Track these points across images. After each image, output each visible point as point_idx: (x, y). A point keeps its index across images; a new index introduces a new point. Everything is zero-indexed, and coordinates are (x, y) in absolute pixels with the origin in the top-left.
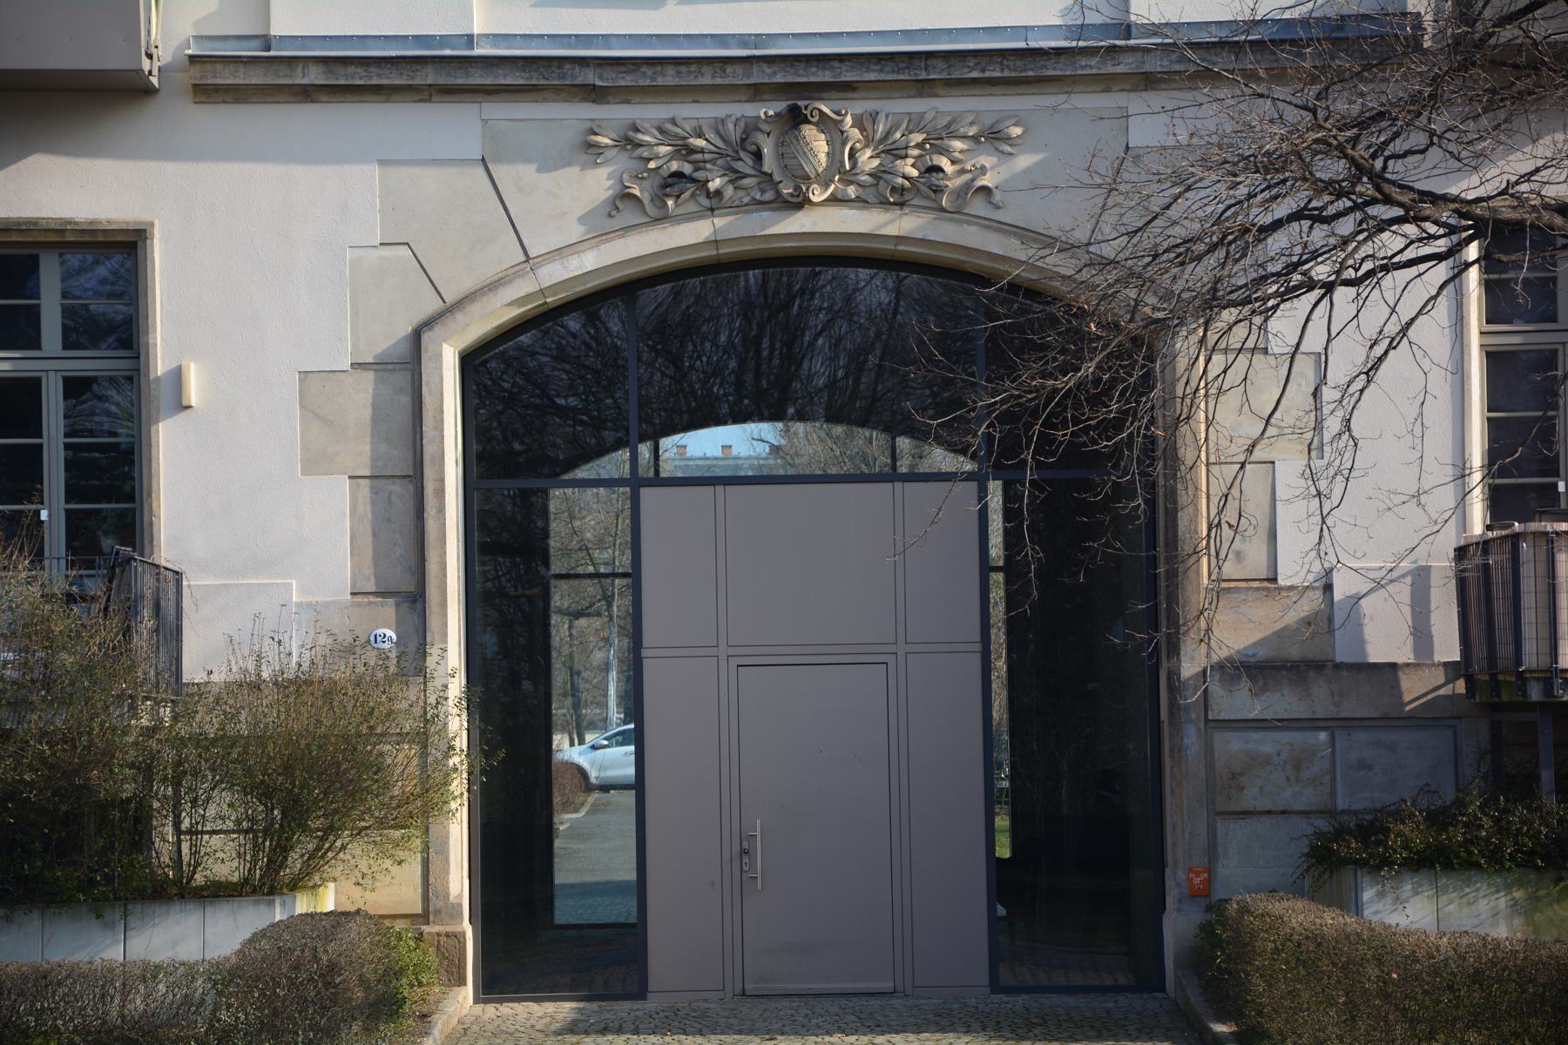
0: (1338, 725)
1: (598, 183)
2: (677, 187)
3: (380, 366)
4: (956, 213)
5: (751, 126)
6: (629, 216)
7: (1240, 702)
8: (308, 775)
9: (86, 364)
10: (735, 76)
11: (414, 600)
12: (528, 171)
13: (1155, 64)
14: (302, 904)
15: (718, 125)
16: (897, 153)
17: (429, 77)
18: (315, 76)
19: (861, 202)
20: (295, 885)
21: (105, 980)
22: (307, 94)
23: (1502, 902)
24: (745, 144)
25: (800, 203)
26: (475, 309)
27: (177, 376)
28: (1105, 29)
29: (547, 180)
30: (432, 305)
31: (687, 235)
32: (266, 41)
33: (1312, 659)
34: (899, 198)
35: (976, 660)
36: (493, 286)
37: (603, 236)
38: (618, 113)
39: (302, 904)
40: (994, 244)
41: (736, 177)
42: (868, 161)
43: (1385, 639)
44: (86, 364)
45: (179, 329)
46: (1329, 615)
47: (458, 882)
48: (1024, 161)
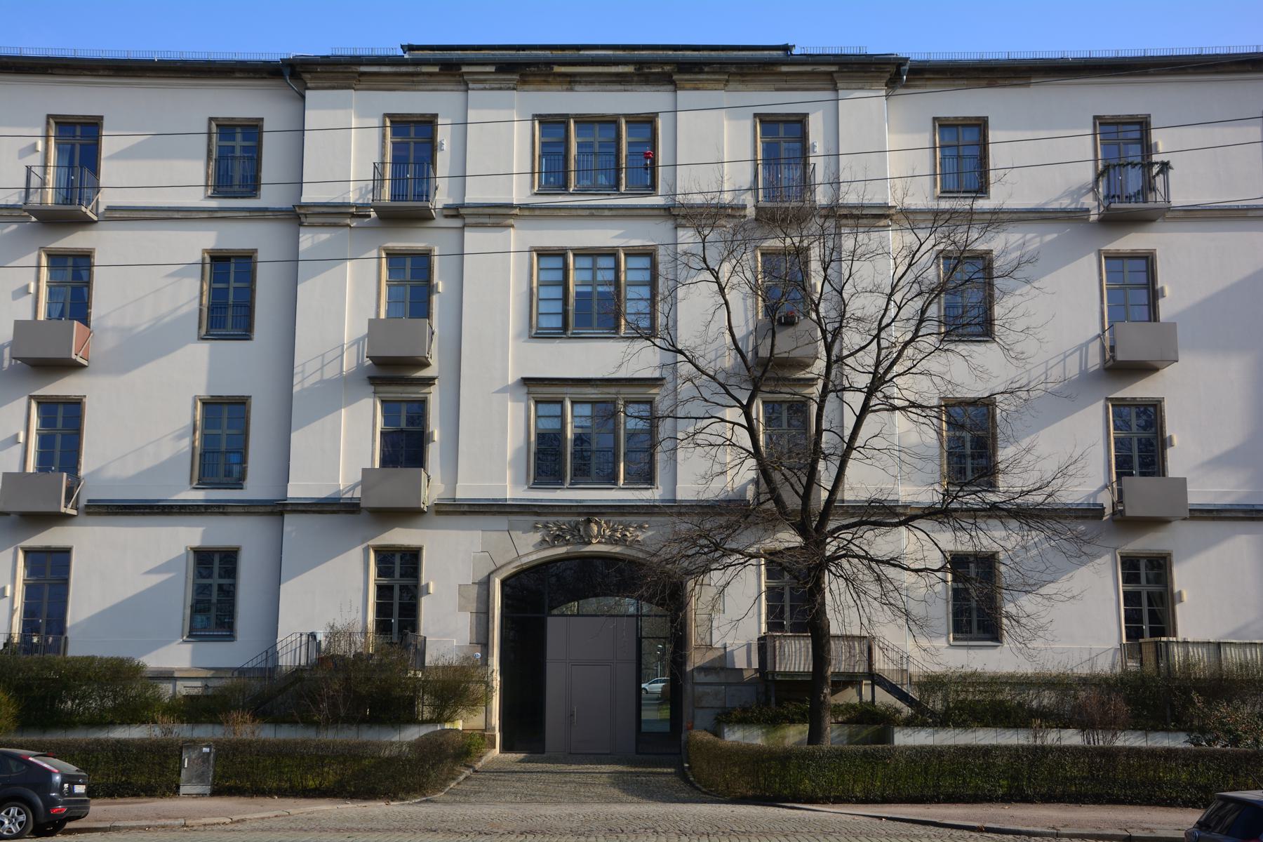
0: (727, 684)
1: (537, 537)
2: (558, 539)
3: (480, 583)
4: (630, 546)
5: (578, 523)
6: (545, 545)
7: (700, 678)
8: (454, 690)
9: (406, 582)
10: (573, 510)
11: (485, 645)
12: (519, 533)
13: (683, 510)
14: (448, 726)
15: (569, 523)
16: (616, 531)
17: (495, 509)
18: (466, 509)
19: (606, 543)
20: (446, 721)
21: (380, 746)
22: (464, 513)
23: (760, 732)
24: (575, 528)
25: (590, 543)
26: (504, 569)
27: (427, 585)
28: (669, 501)
29: (525, 536)
30: (493, 567)
31: (561, 550)
32: (455, 500)
33: (721, 667)
34: (616, 542)
35: (634, 666)
36: (509, 563)
37: (539, 551)
38: (544, 519)
39: (448, 726)
40: (641, 555)
41: (573, 536)
42: (608, 532)
43: (740, 662)
44: (406, 582)
45: (427, 575)
46: (726, 656)
47: (496, 721)
48: (650, 533)
